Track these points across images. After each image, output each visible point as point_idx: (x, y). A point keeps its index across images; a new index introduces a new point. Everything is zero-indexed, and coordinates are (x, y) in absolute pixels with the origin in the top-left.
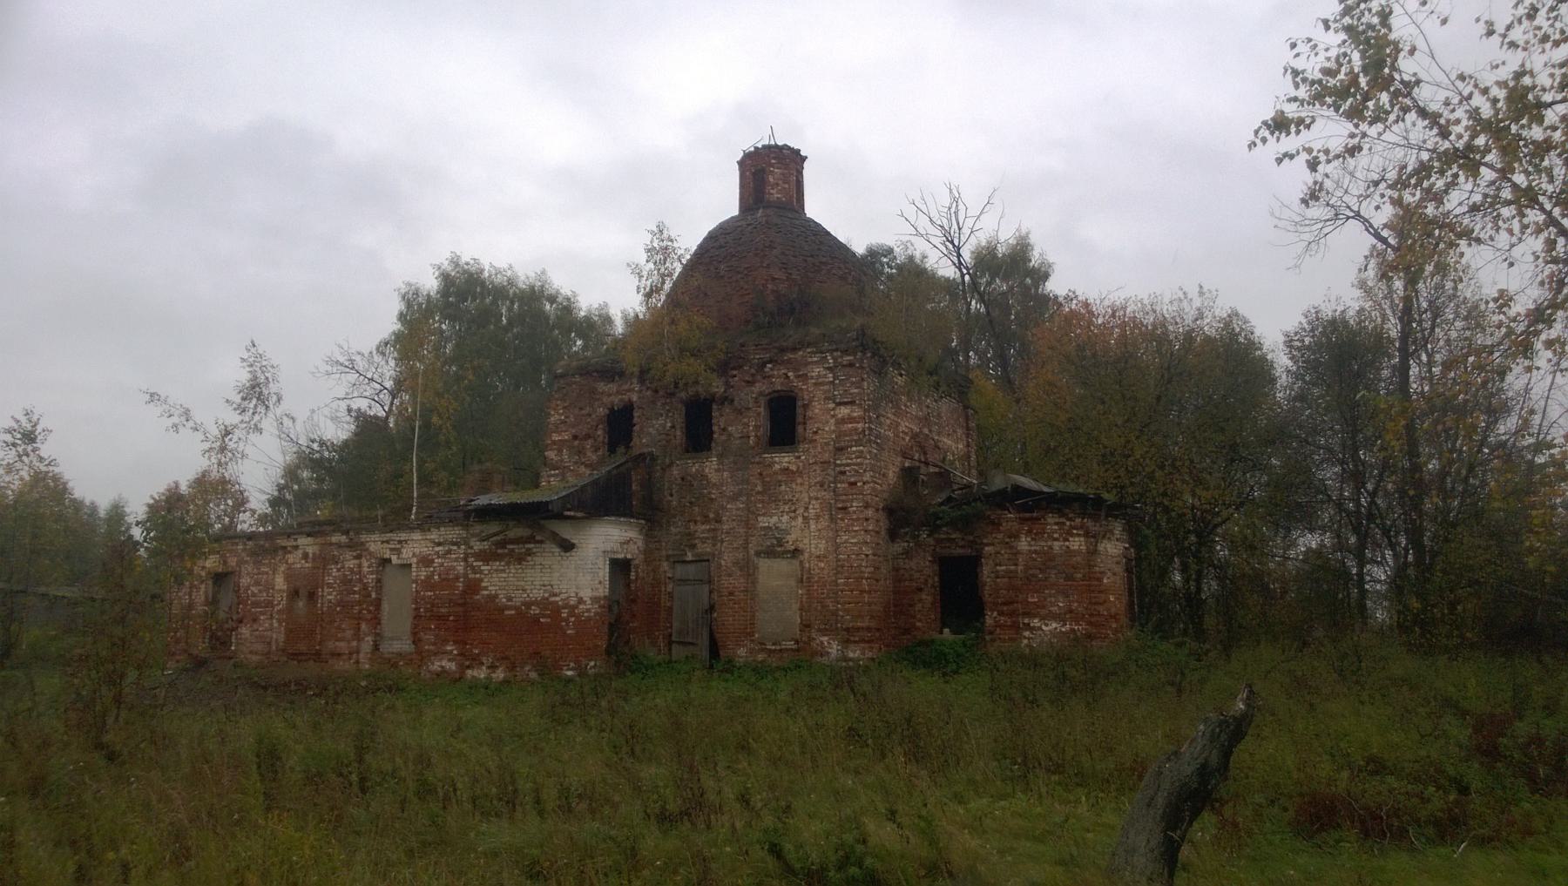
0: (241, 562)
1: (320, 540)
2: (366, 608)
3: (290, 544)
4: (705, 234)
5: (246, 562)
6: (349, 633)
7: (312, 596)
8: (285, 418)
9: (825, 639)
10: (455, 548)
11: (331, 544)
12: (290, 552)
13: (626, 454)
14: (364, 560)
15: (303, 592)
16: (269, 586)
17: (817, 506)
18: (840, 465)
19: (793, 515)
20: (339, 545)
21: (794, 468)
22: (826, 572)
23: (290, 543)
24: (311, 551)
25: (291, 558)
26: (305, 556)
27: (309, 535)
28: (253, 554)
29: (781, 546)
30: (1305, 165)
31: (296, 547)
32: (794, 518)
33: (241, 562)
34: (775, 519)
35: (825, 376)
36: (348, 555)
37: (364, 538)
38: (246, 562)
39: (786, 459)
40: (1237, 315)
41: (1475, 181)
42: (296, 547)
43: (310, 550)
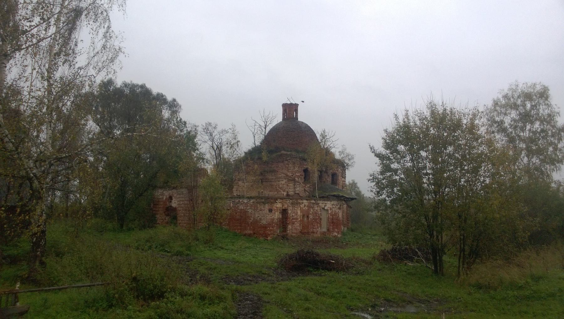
0: (288, 206)
1: (309, 201)
2: (318, 220)
4: (282, 107)
5: (290, 206)
6: (316, 227)
7: (308, 217)
8: (38, 167)
11: (311, 203)
12: (301, 204)
13: (329, 176)
20: (313, 203)
23: (301, 202)
25: (302, 206)
26: (305, 206)
27: (307, 200)
28: (292, 204)
31: (303, 203)
33: (288, 206)
37: (319, 202)
38: (290, 206)
40: (210, 124)
41: (514, 177)
42: (303, 203)
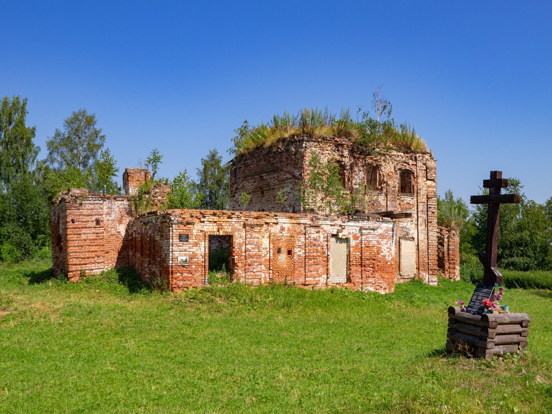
3: (273, 221)
9: (424, 274)
10: (372, 231)
14: (321, 233)
15: (284, 250)
16: (258, 246)
17: (421, 220)
18: (430, 205)
19: (411, 222)
21: (411, 203)
22: (424, 247)
24: (286, 227)
29: (408, 235)
30: (205, 155)
32: (412, 224)
34: (405, 224)
35: (422, 167)
36: (313, 230)
39: (409, 199)
43: (286, 226)
